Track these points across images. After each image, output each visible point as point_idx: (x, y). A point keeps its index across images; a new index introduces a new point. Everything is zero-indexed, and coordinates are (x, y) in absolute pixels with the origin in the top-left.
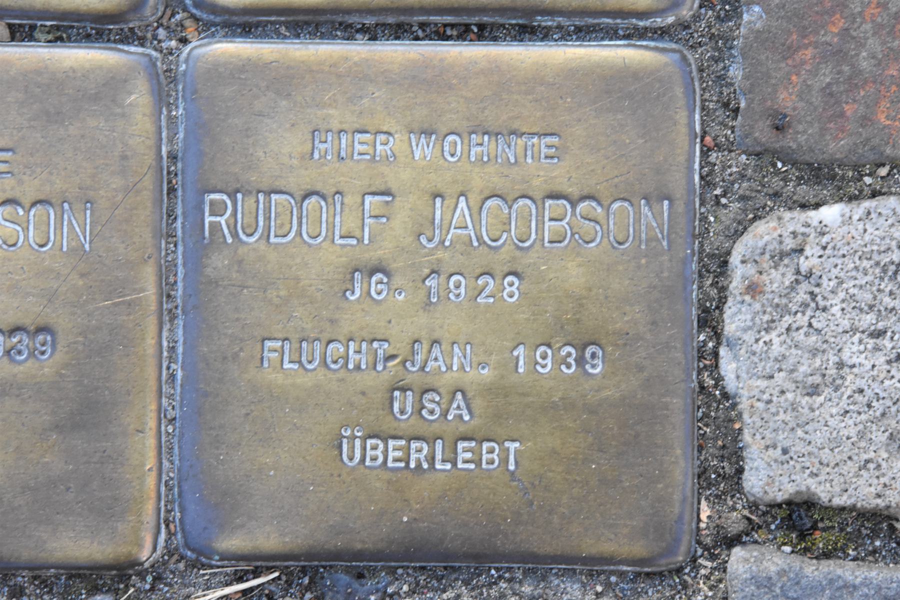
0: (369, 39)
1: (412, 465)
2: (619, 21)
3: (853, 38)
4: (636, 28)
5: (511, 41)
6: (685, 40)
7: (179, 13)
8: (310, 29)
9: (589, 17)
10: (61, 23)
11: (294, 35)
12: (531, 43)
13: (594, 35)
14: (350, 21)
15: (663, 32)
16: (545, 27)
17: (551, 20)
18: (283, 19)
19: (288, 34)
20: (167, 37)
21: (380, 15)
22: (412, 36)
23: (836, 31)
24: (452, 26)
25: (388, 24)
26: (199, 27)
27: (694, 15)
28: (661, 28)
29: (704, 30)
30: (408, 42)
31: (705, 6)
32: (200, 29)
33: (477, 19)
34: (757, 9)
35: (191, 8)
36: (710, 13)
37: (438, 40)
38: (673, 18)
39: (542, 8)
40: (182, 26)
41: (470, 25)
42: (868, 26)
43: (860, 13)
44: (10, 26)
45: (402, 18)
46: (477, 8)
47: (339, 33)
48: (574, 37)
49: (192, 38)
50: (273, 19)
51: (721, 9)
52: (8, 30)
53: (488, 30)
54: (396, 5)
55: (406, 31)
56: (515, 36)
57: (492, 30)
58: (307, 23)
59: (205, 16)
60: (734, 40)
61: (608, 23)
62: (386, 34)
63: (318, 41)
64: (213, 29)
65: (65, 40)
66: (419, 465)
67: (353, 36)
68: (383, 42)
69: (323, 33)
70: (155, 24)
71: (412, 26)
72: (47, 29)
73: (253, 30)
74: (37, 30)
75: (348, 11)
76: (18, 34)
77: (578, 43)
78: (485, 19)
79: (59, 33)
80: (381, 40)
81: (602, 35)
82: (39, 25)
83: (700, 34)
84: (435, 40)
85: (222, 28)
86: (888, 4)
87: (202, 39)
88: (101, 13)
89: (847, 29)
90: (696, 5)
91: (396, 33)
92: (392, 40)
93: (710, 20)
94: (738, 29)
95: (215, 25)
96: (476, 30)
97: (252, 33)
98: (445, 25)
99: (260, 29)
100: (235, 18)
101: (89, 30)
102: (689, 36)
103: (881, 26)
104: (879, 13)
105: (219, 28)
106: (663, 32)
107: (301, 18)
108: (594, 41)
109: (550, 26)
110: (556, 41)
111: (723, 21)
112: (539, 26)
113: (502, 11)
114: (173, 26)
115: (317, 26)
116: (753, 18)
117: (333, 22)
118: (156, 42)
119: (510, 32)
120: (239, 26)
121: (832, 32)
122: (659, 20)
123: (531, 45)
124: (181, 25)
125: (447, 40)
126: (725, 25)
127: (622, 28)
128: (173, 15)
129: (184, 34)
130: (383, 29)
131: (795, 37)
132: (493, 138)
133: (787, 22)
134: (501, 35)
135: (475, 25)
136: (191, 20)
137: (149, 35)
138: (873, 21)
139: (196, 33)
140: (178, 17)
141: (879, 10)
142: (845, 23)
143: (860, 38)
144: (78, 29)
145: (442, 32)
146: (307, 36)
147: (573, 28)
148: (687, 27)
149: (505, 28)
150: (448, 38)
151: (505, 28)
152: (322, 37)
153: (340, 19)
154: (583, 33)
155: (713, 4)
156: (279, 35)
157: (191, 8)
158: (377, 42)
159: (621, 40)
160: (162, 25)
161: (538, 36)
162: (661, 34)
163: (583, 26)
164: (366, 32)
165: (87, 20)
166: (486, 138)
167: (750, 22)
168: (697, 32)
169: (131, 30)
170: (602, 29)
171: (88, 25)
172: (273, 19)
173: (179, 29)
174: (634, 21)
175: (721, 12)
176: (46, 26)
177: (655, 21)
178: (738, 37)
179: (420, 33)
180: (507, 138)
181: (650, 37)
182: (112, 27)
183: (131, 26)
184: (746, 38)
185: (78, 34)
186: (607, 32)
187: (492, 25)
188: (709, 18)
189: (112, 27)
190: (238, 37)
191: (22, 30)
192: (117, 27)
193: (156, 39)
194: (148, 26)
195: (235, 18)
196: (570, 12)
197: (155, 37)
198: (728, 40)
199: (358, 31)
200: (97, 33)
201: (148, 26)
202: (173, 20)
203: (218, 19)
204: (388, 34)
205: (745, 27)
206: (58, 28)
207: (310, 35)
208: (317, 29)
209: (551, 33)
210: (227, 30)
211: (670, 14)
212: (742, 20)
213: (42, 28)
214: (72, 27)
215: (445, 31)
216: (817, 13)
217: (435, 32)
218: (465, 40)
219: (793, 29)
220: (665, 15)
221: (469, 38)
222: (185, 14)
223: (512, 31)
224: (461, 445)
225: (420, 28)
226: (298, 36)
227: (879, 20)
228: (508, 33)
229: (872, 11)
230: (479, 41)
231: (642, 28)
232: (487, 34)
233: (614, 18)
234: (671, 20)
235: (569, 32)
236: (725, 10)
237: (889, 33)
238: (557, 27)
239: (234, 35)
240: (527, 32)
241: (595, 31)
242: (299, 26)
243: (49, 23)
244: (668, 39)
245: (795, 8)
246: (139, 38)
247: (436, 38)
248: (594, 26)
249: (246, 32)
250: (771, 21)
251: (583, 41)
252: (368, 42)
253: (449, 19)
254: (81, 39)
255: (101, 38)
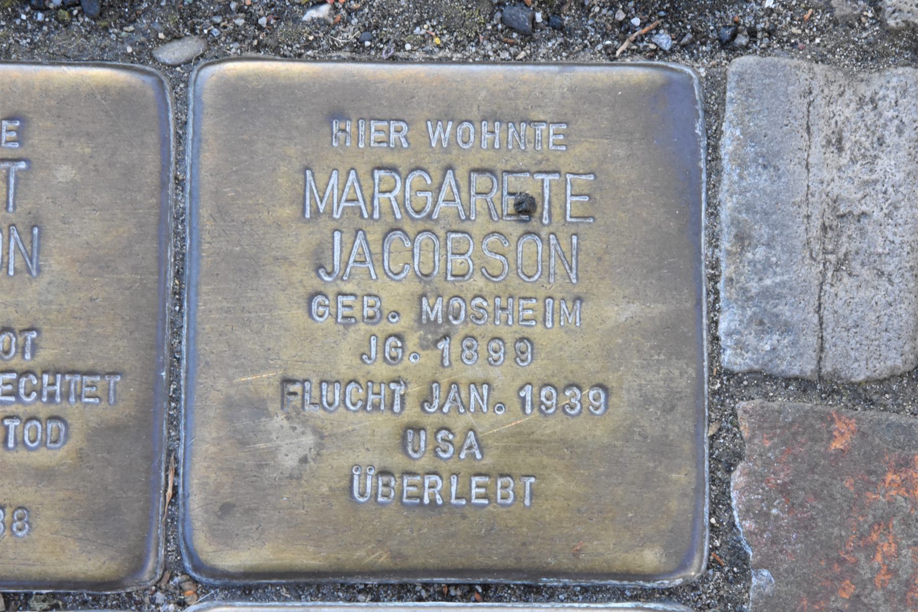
0: (372, 600)
1: (426, 501)
2: (625, 582)
3: (865, 605)
4: (643, 589)
5: (517, 601)
6: (693, 601)
7: (177, 575)
8: (311, 591)
9: (595, 579)
10: (58, 591)
11: (296, 597)
12: (537, 605)
13: (601, 596)
14: (352, 582)
15: (671, 593)
16: (551, 587)
17: (556, 582)
18: (284, 581)
19: (289, 596)
20: (165, 600)
21: (383, 577)
22: (415, 596)
23: (847, 597)
24: (456, 586)
25: (391, 585)
26: (198, 590)
27: (702, 576)
28: (668, 589)
29: (712, 592)
30: (411, 604)
31: (713, 567)
32: (199, 592)
33: (481, 580)
34: (765, 573)
35: (190, 571)
36: (718, 574)
37: (442, 601)
38: (681, 580)
39: (548, 569)
40: (181, 588)
41: (475, 585)
42: (879, 593)
43: (871, 580)
44: (5, 595)
45: (405, 580)
46: (481, 569)
47: (341, 594)
48: (581, 597)
49: (191, 601)
50: (274, 581)
51: (728, 571)
52: (2, 600)
53: (493, 589)
54: (399, 567)
55: (409, 591)
56: (521, 596)
57: (496, 589)
58: (309, 585)
59: (204, 579)
60: (744, 604)
61: (614, 585)
62: (388, 595)
63: (320, 603)
64: (213, 592)
65: (61, 607)
66: (433, 502)
67: (355, 597)
68: (385, 604)
69: (325, 594)
70: (154, 588)
71: (415, 586)
72: (42, 597)
73: (253, 592)
74: (33, 599)
75: (351, 574)
76: (13, 603)
77: (585, 605)
78: (490, 580)
79: (55, 601)
80: (384, 601)
81: (609, 595)
82: (34, 593)
83: (708, 595)
84: (439, 601)
85: (221, 590)
86: (898, 571)
87: (201, 602)
88: (99, 581)
89: (858, 596)
90: (704, 566)
91: (399, 593)
92: (395, 601)
93: (719, 581)
94: (747, 592)
95: (214, 587)
96: (480, 590)
97: (252, 595)
98: (449, 585)
99: (260, 591)
100: (235, 582)
101: (86, 597)
102: (697, 597)
103: (892, 593)
104: (890, 580)
105: (218, 590)
106: (671, 593)
107: (303, 580)
108: (600, 602)
109: (555, 586)
110: (562, 601)
111: (731, 583)
112: (545, 586)
113: (506, 572)
114: (171, 590)
115: (319, 587)
116: (762, 583)
117: (335, 583)
118: (153, 606)
119: (515, 592)
120: (239, 588)
121: (843, 598)
122: (666, 582)
123: (537, 608)
124: (179, 587)
125: (451, 601)
126: (734, 587)
127: (629, 589)
128: (171, 578)
129: (182, 597)
130: (385, 589)
131: (805, 602)
132: (504, 126)
133: (797, 587)
134: (506, 595)
135: (480, 585)
136: (190, 582)
137: (147, 600)
138: (883, 588)
139: (195, 596)
140: (177, 579)
141: (889, 577)
142: (855, 590)
143: (871, 605)
144: (74, 596)
145: (446, 592)
146: (309, 598)
147: (579, 588)
148: (695, 588)
149: (509, 588)
150: (451, 599)
151: (509, 588)
152: (324, 599)
153: (342, 581)
154: (590, 593)
155: (720, 565)
156: (280, 597)
157: (190, 571)
158: (380, 604)
159: (628, 601)
160: (160, 588)
161: (543, 596)
162: (669, 595)
163: (589, 587)
164: (368, 593)
165: (84, 588)
166: (497, 124)
167: (759, 587)
168: (706, 593)
169: (129, 595)
170: (608, 590)
171: (85, 592)
172: (274, 581)
173: (178, 592)
174: (641, 583)
175: (729, 574)
176: (41, 594)
177: (662, 583)
178: (747, 601)
179: (424, 594)
180: (517, 125)
181: (657, 598)
182: (109, 593)
183: (128, 590)
184: (756, 604)
185: (75, 601)
186: (614, 593)
187: (497, 585)
188: (717, 579)
189: (109, 593)
190: (238, 600)
191: (17, 598)
192: (114, 592)
193: (154, 603)
194: (146, 590)
195: (235, 582)
196: (576, 574)
197: (153, 601)
198: (737, 603)
199: (360, 592)
200: (94, 600)
201: (146, 590)
202: (171, 583)
203: (218, 582)
204: (391, 595)
205: (754, 592)
206: (54, 595)
207: (312, 596)
208: (319, 591)
209: (557, 593)
210: (226, 592)
211: (678, 576)
212: (751, 583)
213: (38, 596)
214: (69, 594)
215: (449, 591)
216: (827, 578)
217: (438, 592)
218: (469, 601)
219: (803, 595)
220: (672, 577)
221: (473, 598)
222: (184, 577)
223: (517, 591)
224: (475, 480)
225: (423, 588)
226: (299, 598)
227: (890, 587)
228: (513, 593)
229: (883, 578)
230: (484, 601)
231: (649, 590)
232: (491, 594)
233: (621, 580)
234: (678, 582)
235: (575, 592)
236: (733, 572)
237: (901, 601)
238: (563, 587)
239: (234, 598)
240: (533, 592)
241: (601, 591)
242: (300, 588)
243: (44, 592)
244: (676, 600)
245: (804, 573)
246: (136, 603)
247: (440, 598)
248: (600, 586)
249: (246, 594)
250: (780, 586)
251: (590, 602)
252: (371, 604)
253: (452, 580)
254: (78, 606)
255: (98, 604)
